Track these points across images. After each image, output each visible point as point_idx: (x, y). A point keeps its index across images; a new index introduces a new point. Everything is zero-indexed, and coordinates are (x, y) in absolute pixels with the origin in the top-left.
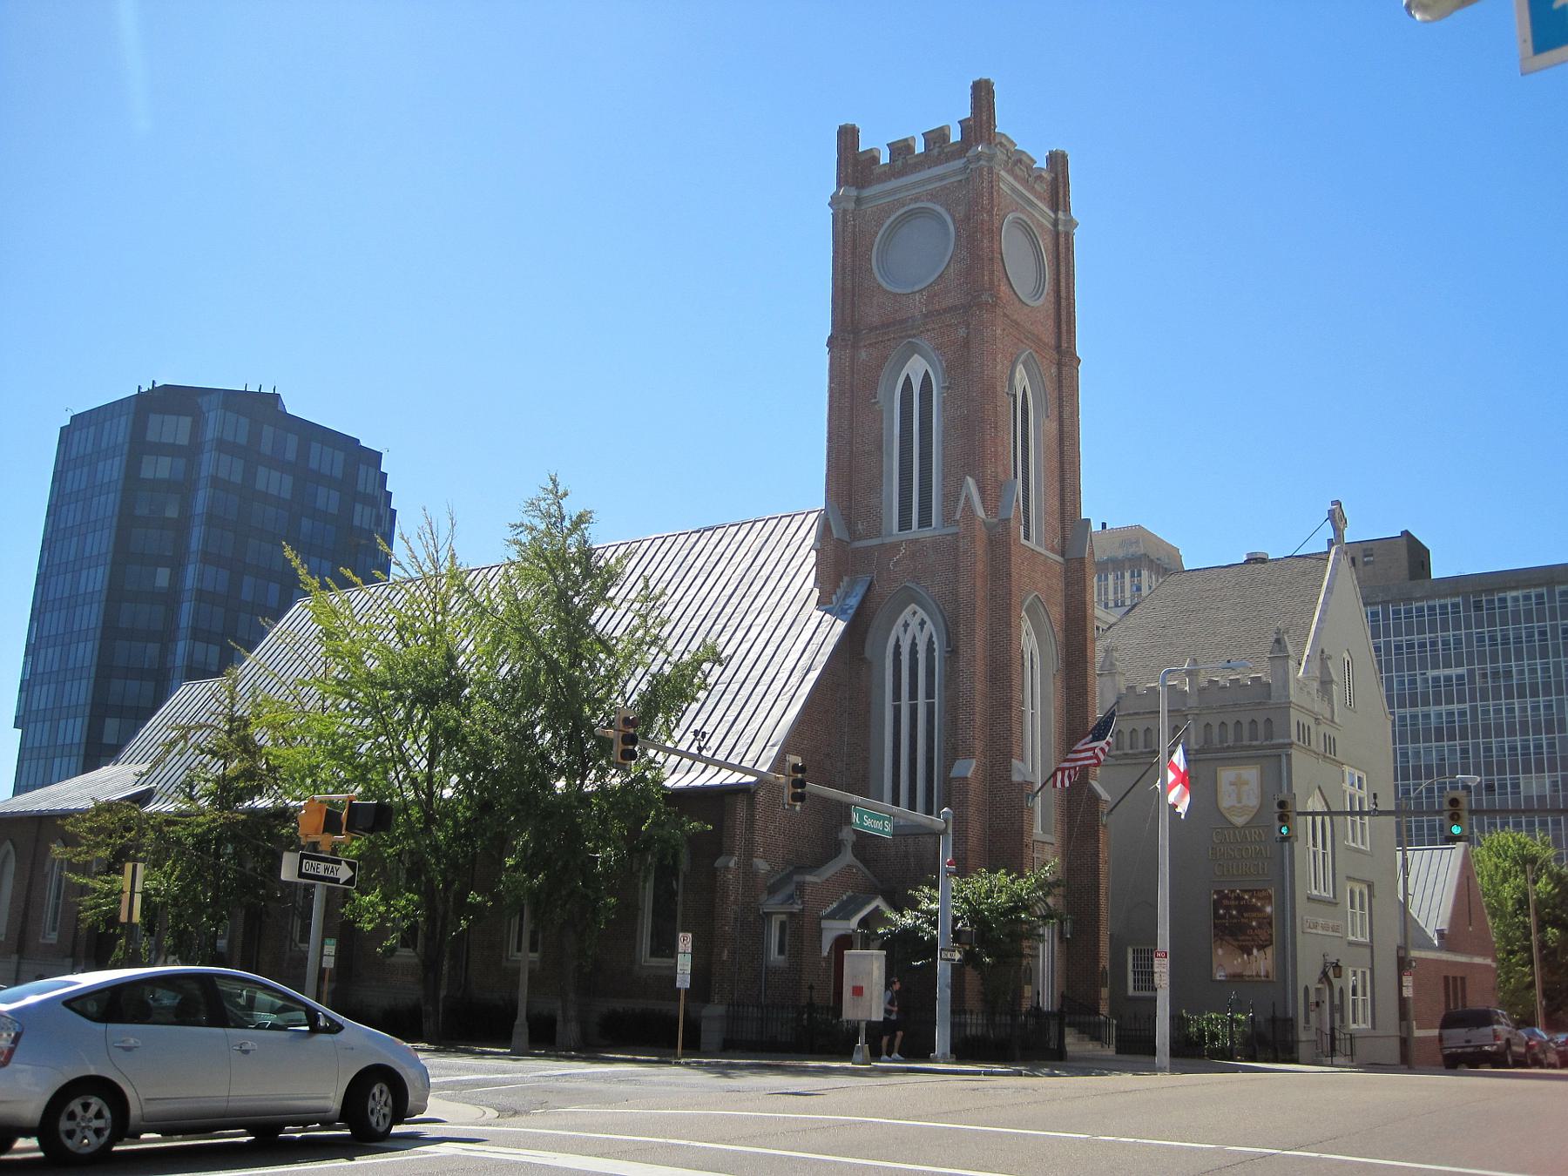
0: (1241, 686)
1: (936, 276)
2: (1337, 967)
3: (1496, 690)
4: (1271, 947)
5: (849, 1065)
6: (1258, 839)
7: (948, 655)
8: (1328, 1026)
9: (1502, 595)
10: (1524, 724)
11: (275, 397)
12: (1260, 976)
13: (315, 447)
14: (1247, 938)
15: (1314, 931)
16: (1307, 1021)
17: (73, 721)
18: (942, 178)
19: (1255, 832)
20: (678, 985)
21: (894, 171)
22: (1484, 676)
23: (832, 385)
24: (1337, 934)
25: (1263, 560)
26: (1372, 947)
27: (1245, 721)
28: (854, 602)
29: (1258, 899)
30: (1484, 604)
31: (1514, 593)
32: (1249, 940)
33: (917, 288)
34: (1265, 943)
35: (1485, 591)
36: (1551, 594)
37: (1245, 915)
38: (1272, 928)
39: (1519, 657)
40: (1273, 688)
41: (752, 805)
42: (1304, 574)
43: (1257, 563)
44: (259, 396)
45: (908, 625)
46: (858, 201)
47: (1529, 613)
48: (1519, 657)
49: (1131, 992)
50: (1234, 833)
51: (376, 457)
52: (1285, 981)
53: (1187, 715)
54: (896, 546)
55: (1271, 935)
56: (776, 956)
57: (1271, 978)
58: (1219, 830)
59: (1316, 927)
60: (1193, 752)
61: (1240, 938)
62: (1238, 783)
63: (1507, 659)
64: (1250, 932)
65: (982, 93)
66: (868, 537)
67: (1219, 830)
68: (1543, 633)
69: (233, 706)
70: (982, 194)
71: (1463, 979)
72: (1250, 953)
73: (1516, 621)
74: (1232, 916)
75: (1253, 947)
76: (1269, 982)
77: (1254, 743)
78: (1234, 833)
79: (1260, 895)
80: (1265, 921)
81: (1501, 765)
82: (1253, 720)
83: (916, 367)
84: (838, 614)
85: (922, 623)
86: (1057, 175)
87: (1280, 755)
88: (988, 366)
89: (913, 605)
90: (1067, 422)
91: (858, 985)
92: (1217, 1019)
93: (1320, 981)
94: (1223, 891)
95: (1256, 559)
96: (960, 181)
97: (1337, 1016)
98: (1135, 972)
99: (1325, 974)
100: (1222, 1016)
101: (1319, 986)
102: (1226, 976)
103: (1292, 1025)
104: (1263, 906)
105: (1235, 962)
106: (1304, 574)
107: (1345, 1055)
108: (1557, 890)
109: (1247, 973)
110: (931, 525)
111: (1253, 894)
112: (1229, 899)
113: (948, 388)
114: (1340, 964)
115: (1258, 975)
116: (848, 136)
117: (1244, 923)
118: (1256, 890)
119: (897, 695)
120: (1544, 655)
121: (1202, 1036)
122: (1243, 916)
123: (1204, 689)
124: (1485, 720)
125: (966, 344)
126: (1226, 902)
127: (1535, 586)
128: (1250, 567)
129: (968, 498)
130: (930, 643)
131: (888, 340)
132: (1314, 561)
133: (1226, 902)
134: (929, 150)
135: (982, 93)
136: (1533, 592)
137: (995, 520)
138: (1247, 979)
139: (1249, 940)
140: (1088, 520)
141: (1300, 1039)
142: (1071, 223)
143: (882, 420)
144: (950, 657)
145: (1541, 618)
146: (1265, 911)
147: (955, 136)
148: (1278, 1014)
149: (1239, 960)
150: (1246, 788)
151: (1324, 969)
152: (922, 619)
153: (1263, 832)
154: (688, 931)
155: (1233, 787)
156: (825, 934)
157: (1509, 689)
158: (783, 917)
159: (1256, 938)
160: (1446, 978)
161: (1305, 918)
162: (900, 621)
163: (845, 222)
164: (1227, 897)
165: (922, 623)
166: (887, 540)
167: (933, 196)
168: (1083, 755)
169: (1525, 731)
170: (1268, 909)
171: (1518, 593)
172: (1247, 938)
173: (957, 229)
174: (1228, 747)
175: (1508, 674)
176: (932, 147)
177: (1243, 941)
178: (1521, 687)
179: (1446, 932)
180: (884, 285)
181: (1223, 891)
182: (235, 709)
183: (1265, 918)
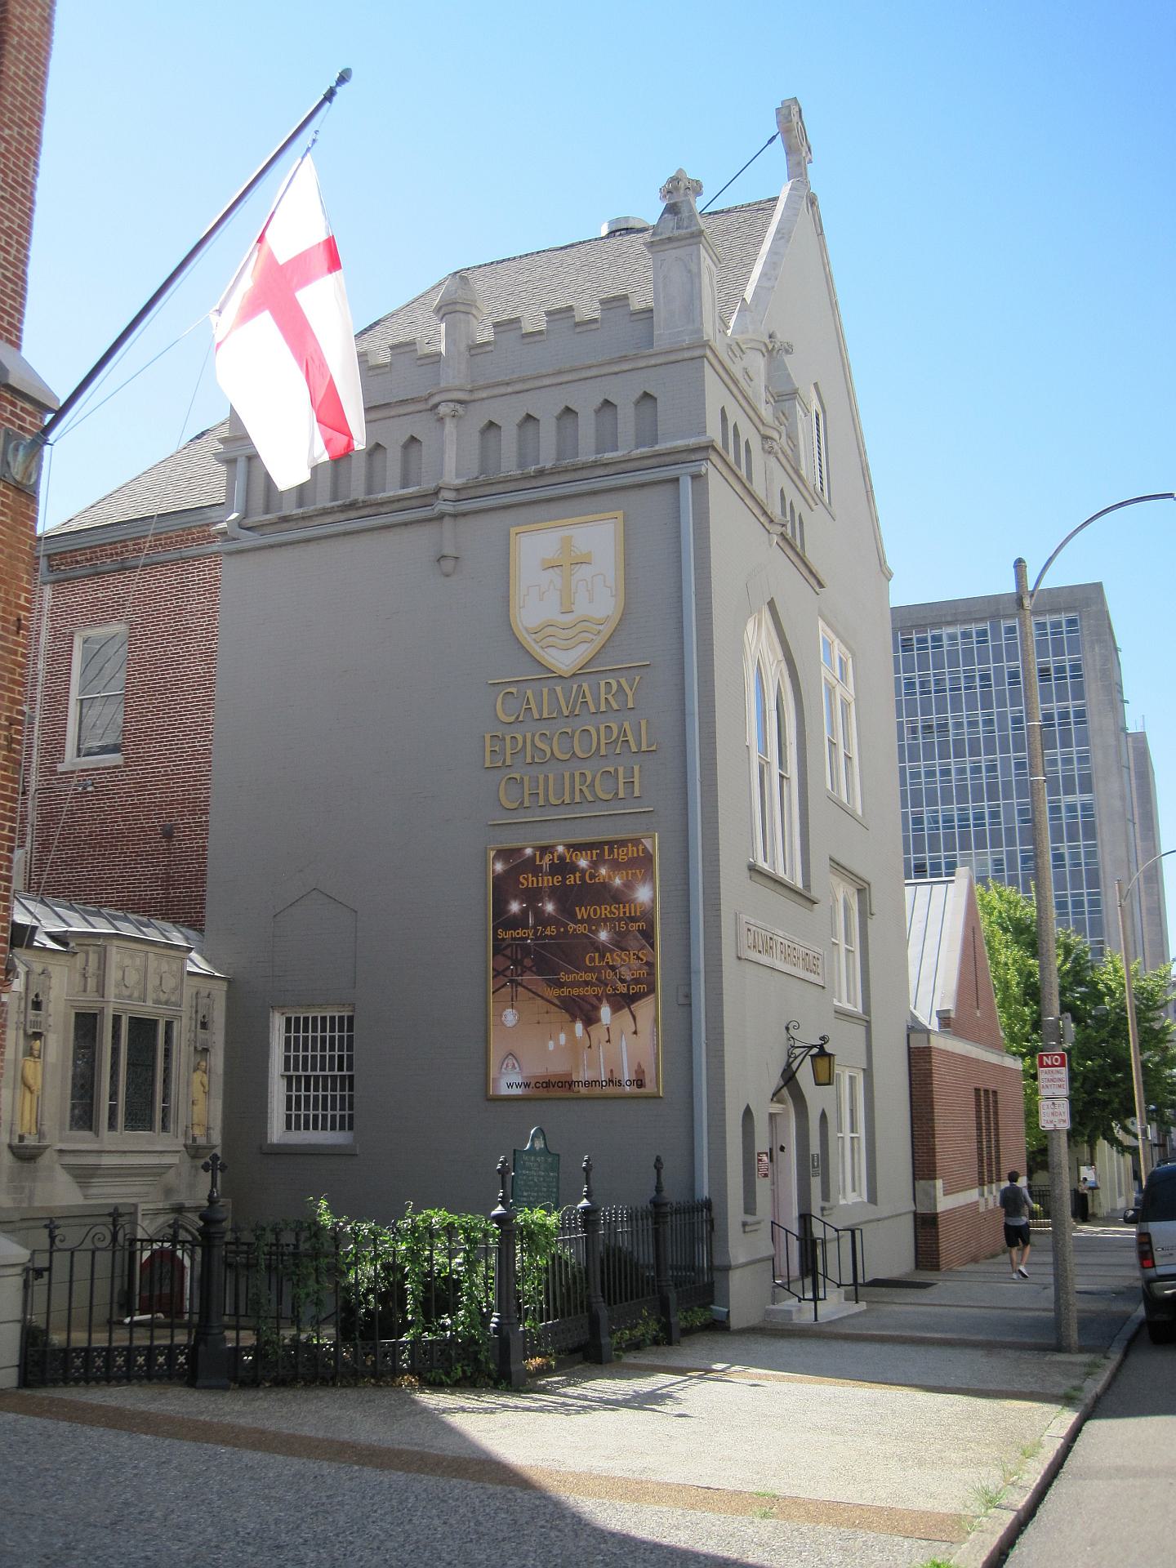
0: (577, 324)
2: (822, 1055)
3: (929, 747)
4: (650, 999)
8: (795, 1214)
9: (936, 632)
10: (962, 789)
14: (588, 977)
15: (764, 959)
16: (750, 1207)
22: (914, 730)
24: (812, 977)
26: (868, 1026)
27: (587, 406)
29: (616, 865)
30: (915, 643)
31: (951, 630)
32: (587, 983)
35: (913, 627)
36: (995, 629)
37: (581, 913)
38: (652, 946)
39: (956, 707)
47: (968, 653)
48: (956, 707)
49: (277, 1132)
50: (552, 691)
53: (436, 406)
55: (651, 965)
57: (650, 1088)
58: (513, 690)
59: (768, 950)
60: (451, 495)
61: (563, 977)
62: (568, 563)
63: (941, 709)
64: (591, 959)
67: (513, 690)
68: (985, 677)
71: (995, 1092)
72: (590, 1020)
73: (953, 663)
74: (543, 920)
75: (600, 1000)
76: (647, 1097)
77: (609, 456)
78: (552, 691)
79: (622, 855)
80: (634, 927)
81: (934, 839)
82: (607, 403)
93: (776, 1096)
94: (520, 850)
97: (816, 1183)
98: (289, 1078)
99: (789, 1077)
100: (467, 1219)
101: (776, 1108)
102: (527, 1085)
103: (711, 1222)
104: (629, 885)
105: (551, 1045)
107: (839, 1286)
108: (1068, 965)
109: (585, 1075)
111: (600, 856)
112: (536, 870)
114: (828, 1048)
117: (575, 936)
118: (610, 843)
120: (987, 704)
121: (393, 1296)
122: (573, 917)
124: (957, 734)
126: (527, 881)
127: (977, 620)
133: (527, 881)
136: (974, 628)
138: (583, 1090)
139: (587, 983)
141: (733, 1263)
145: (983, 660)
146: (631, 901)
148: (673, 1195)
149: (562, 1038)
150: (583, 572)
151: (789, 1065)
155: (552, 574)
157: (944, 745)
159: (609, 975)
160: (977, 1090)
161: (744, 918)
164: (531, 866)
169: (962, 798)
170: (643, 894)
171: (957, 630)
172: (588, 977)
174: (541, 473)
175: (943, 727)
177: (572, 985)
178: (958, 743)
179: (953, 1015)
181: (520, 850)
183: (633, 919)
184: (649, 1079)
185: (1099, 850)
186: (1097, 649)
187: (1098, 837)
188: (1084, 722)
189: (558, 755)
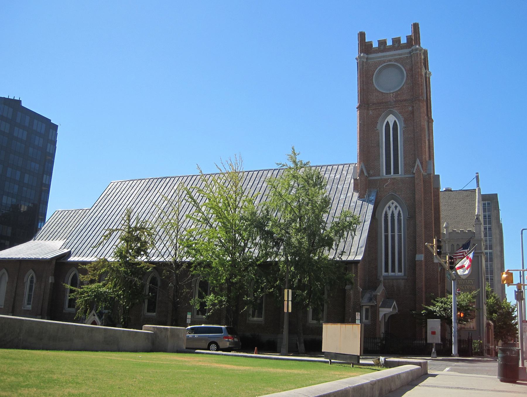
1: (399, 88)
5: (430, 358)
6: (470, 283)
7: (408, 218)
11: (19, 102)
12: (471, 328)
13: (36, 122)
17: (40, 224)
18: (401, 54)
19: (469, 281)
20: (187, 322)
21: (378, 50)
23: (360, 122)
25: (451, 191)
28: (373, 198)
33: (391, 92)
34: (473, 317)
40: (476, 234)
41: (356, 268)
42: (467, 196)
43: (449, 191)
44: (14, 100)
45: (390, 207)
46: (367, 59)
51: (55, 127)
52: (480, 330)
53: (445, 241)
54: (386, 180)
56: (364, 320)
57: (475, 329)
65: (416, 27)
66: (375, 176)
69: (129, 221)
70: (418, 62)
83: (391, 119)
84: (369, 202)
85: (396, 207)
86: (425, 57)
87: (478, 256)
88: (422, 121)
89: (393, 200)
90: (431, 141)
91: (434, 331)
92: (476, 342)
95: (448, 190)
96: (408, 56)
106: (467, 196)
110: (398, 174)
113: (405, 127)
115: (470, 328)
116: (362, 35)
119: (386, 230)
123: (451, 233)
125: (412, 112)
128: (447, 192)
129: (418, 166)
130: (399, 214)
131: (380, 108)
132: (470, 192)
134: (394, 45)
135: (416, 27)
137: (426, 174)
138: (466, 329)
140: (438, 176)
142: (430, 73)
143: (379, 135)
144: (409, 219)
147: (404, 41)
152: (396, 206)
153: (472, 281)
154: (359, 312)
156: (380, 313)
158: (368, 307)
162: (387, 206)
163: (363, 66)
165: (396, 207)
166: (382, 178)
167: (396, 60)
168: (458, 254)
173: (406, 73)
176: (395, 43)
180: (378, 89)
182: (131, 223)
184: (475, 328)
185: (493, 265)
186: (495, 212)
187: (493, 261)
188: (491, 231)
189: (463, 289)
